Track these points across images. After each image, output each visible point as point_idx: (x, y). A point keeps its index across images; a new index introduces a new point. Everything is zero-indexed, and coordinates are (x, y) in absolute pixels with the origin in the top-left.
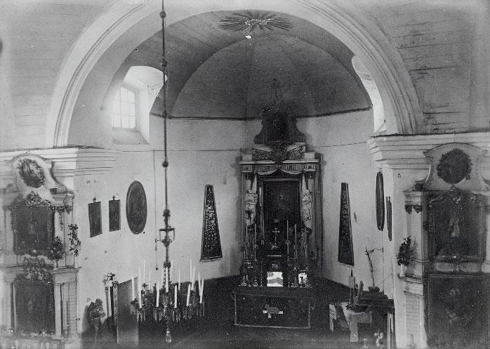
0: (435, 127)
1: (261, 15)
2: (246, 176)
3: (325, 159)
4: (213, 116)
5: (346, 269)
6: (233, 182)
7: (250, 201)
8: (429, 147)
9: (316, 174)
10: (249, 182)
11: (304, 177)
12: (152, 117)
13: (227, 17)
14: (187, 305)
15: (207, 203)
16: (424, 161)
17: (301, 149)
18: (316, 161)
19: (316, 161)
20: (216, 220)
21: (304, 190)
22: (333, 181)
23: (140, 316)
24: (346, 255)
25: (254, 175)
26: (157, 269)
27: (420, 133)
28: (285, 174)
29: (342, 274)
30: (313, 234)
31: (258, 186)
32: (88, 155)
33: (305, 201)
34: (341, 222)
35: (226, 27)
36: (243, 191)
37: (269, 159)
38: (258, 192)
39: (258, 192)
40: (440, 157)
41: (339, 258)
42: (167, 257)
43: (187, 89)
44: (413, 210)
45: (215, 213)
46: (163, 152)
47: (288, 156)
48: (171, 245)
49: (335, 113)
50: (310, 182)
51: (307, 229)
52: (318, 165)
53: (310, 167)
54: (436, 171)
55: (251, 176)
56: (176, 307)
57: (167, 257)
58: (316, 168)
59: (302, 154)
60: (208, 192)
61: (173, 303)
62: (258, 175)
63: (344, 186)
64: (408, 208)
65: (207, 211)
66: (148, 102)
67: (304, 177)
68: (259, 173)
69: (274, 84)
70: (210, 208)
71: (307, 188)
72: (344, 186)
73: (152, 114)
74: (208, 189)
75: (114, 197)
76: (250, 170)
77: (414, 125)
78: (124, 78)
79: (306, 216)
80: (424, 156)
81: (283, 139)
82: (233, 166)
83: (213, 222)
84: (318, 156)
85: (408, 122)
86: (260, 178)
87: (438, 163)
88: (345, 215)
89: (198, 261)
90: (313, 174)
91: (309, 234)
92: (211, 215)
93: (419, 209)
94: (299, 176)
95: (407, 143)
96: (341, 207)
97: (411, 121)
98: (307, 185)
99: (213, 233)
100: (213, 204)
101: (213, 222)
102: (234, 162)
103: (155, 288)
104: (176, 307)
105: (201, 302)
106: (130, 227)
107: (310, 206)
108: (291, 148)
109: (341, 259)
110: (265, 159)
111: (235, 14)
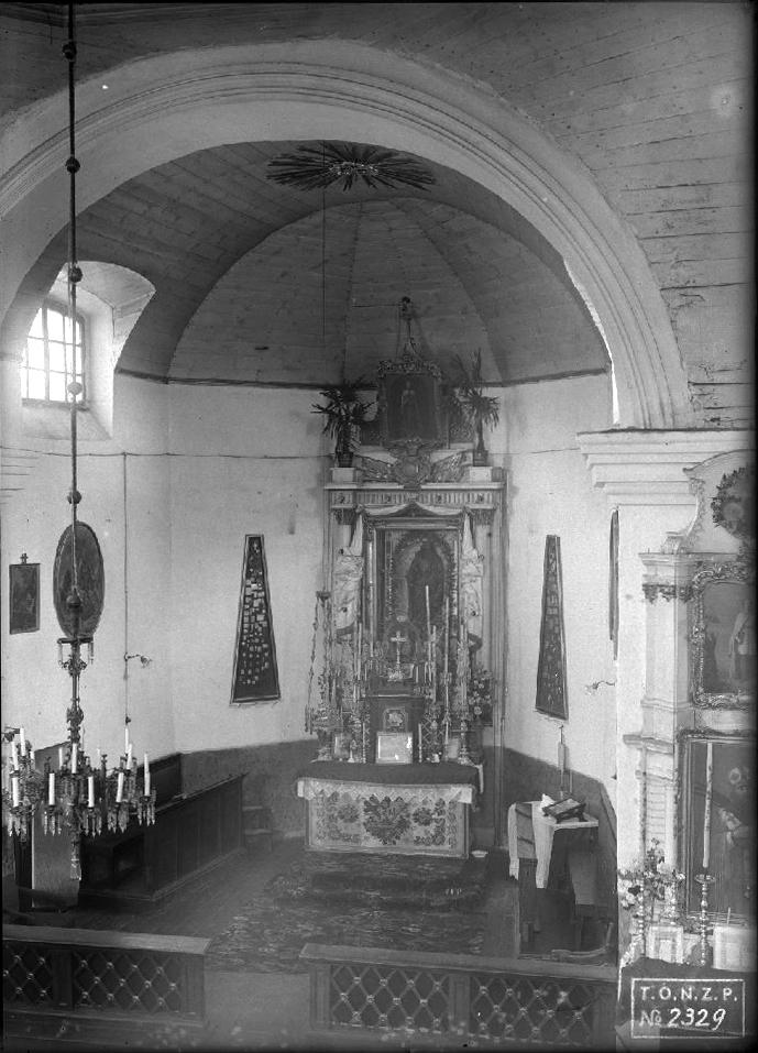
0: (713, 414)
1: (361, 152)
2: (339, 518)
4: (238, 378)
5: (548, 725)
7: (348, 572)
8: (699, 459)
9: (493, 514)
11: (467, 523)
14: (118, 800)
15: (248, 575)
16: (686, 488)
17: (464, 458)
18: (495, 486)
19: (495, 486)
20: (268, 618)
21: (469, 552)
22: (531, 532)
23: (14, 823)
24: (552, 699)
25: (357, 515)
27: (682, 426)
29: (540, 739)
31: (366, 539)
32: (652, 448)
36: (332, 550)
38: (365, 553)
39: (365, 553)
40: (718, 481)
41: (539, 702)
43: (204, 316)
44: (660, 594)
45: (266, 599)
46: (70, 459)
47: (434, 472)
50: (482, 531)
51: (470, 637)
53: (481, 499)
54: (710, 512)
55: (349, 517)
56: (91, 804)
57: (76, 699)
59: (463, 471)
60: (251, 551)
61: (87, 798)
62: (367, 516)
63: (552, 544)
64: (650, 590)
67: (467, 523)
71: (475, 547)
72: (552, 544)
73: (119, 370)
74: (251, 543)
75: (24, 557)
77: (668, 410)
79: (741, 615)
80: (686, 478)
82: (312, 492)
83: (260, 618)
84: (501, 476)
85: (656, 403)
86: (371, 521)
87: (715, 493)
93: (670, 593)
94: (456, 521)
97: (661, 399)
98: (473, 537)
102: (313, 484)
103: (104, 762)
104: (91, 804)
105: (147, 793)
107: (478, 585)
108: (439, 456)
110: (381, 480)
111: (303, 149)
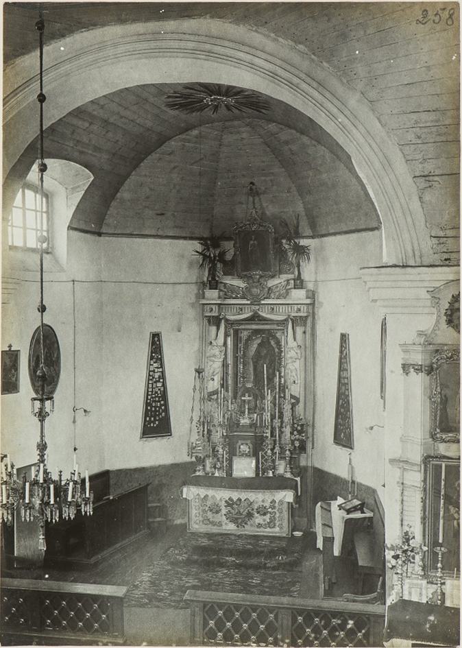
0: (446, 256)
3: (320, 300)
5: (343, 452)
6: (192, 329)
7: (214, 356)
9: (305, 320)
10: (214, 329)
12: (71, 232)
13: (175, 93)
15: (152, 358)
16: (428, 303)
18: (308, 301)
24: (343, 436)
25: (221, 320)
26: (75, 449)
28: (265, 319)
29: (334, 461)
30: (301, 404)
31: (226, 335)
33: (291, 358)
34: (339, 389)
35: (172, 106)
36: (205, 341)
37: (243, 297)
38: (225, 344)
39: (225, 344)
42: (42, 436)
44: (412, 370)
45: (163, 372)
46: (420, 265)
48: (47, 419)
49: (335, 234)
52: (310, 307)
55: (216, 321)
56: (52, 502)
57: (42, 436)
58: (308, 312)
60: (153, 343)
61: (49, 498)
62: (227, 320)
63: (344, 338)
64: (405, 367)
65: (152, 369)
66: (65, 209)
68: (227, 317)
69: (251, 189)
70: (155, 365)
72: (344, 338)
73: (70, 228)
75: (10, 346)
76: (215, 314)
78: (26, 177)
81: (263, 270)
83: (159, 385)
84: (312, 295)
85: (409, 249)
88: (344, 378)
89: (139, 439)
90: (303, 320)
91: (293, 406)
92: (157, 376)
93: (419, 369)
94: (283, 323)
95: (408, 277)
96: (340, 367)
99: (159, 401)
100: (160, 360)
101: (159, 385)
104: (52, 502)
106: (34, 390)
108: (271, 283)
109: (338, 440)
